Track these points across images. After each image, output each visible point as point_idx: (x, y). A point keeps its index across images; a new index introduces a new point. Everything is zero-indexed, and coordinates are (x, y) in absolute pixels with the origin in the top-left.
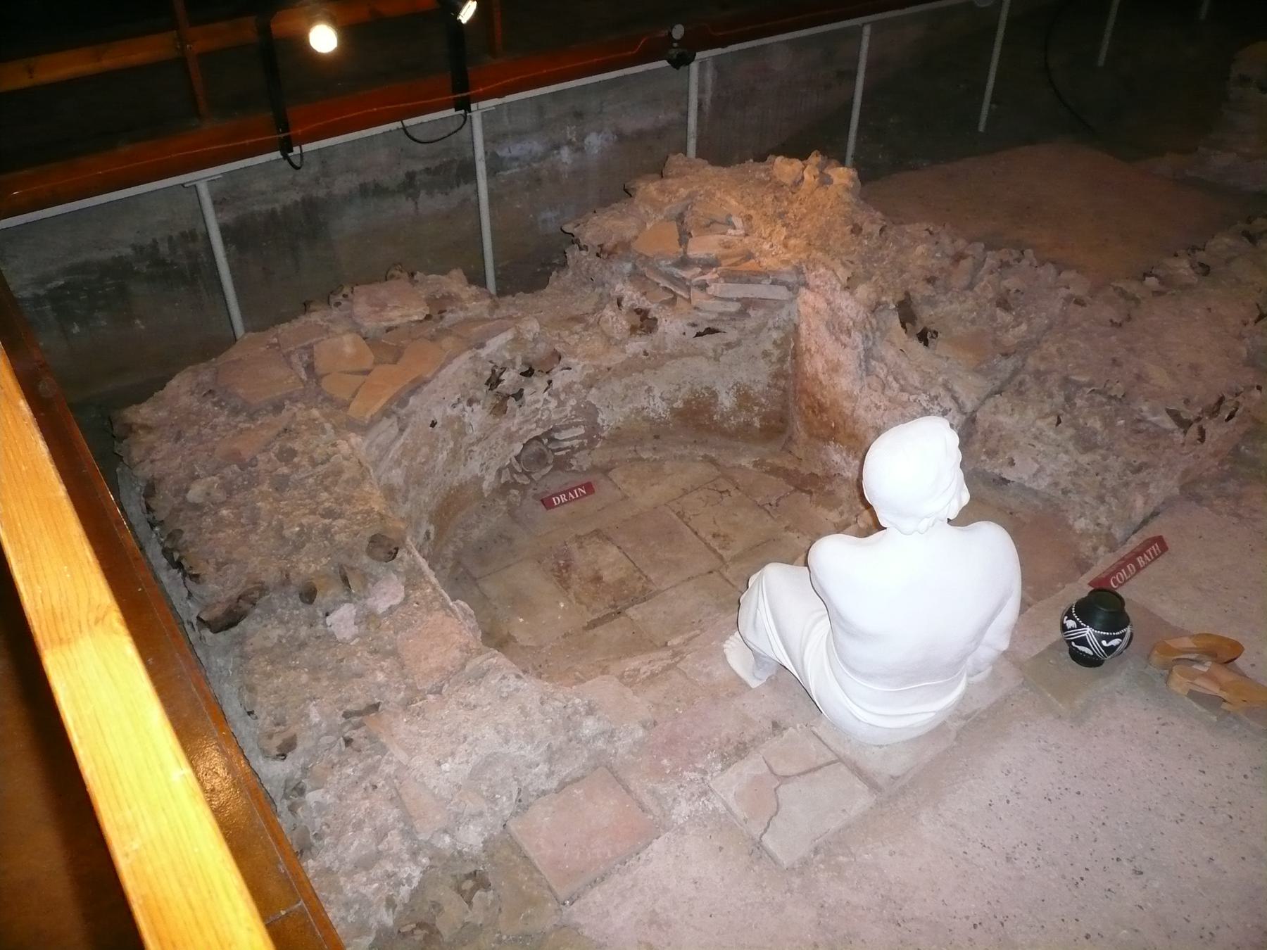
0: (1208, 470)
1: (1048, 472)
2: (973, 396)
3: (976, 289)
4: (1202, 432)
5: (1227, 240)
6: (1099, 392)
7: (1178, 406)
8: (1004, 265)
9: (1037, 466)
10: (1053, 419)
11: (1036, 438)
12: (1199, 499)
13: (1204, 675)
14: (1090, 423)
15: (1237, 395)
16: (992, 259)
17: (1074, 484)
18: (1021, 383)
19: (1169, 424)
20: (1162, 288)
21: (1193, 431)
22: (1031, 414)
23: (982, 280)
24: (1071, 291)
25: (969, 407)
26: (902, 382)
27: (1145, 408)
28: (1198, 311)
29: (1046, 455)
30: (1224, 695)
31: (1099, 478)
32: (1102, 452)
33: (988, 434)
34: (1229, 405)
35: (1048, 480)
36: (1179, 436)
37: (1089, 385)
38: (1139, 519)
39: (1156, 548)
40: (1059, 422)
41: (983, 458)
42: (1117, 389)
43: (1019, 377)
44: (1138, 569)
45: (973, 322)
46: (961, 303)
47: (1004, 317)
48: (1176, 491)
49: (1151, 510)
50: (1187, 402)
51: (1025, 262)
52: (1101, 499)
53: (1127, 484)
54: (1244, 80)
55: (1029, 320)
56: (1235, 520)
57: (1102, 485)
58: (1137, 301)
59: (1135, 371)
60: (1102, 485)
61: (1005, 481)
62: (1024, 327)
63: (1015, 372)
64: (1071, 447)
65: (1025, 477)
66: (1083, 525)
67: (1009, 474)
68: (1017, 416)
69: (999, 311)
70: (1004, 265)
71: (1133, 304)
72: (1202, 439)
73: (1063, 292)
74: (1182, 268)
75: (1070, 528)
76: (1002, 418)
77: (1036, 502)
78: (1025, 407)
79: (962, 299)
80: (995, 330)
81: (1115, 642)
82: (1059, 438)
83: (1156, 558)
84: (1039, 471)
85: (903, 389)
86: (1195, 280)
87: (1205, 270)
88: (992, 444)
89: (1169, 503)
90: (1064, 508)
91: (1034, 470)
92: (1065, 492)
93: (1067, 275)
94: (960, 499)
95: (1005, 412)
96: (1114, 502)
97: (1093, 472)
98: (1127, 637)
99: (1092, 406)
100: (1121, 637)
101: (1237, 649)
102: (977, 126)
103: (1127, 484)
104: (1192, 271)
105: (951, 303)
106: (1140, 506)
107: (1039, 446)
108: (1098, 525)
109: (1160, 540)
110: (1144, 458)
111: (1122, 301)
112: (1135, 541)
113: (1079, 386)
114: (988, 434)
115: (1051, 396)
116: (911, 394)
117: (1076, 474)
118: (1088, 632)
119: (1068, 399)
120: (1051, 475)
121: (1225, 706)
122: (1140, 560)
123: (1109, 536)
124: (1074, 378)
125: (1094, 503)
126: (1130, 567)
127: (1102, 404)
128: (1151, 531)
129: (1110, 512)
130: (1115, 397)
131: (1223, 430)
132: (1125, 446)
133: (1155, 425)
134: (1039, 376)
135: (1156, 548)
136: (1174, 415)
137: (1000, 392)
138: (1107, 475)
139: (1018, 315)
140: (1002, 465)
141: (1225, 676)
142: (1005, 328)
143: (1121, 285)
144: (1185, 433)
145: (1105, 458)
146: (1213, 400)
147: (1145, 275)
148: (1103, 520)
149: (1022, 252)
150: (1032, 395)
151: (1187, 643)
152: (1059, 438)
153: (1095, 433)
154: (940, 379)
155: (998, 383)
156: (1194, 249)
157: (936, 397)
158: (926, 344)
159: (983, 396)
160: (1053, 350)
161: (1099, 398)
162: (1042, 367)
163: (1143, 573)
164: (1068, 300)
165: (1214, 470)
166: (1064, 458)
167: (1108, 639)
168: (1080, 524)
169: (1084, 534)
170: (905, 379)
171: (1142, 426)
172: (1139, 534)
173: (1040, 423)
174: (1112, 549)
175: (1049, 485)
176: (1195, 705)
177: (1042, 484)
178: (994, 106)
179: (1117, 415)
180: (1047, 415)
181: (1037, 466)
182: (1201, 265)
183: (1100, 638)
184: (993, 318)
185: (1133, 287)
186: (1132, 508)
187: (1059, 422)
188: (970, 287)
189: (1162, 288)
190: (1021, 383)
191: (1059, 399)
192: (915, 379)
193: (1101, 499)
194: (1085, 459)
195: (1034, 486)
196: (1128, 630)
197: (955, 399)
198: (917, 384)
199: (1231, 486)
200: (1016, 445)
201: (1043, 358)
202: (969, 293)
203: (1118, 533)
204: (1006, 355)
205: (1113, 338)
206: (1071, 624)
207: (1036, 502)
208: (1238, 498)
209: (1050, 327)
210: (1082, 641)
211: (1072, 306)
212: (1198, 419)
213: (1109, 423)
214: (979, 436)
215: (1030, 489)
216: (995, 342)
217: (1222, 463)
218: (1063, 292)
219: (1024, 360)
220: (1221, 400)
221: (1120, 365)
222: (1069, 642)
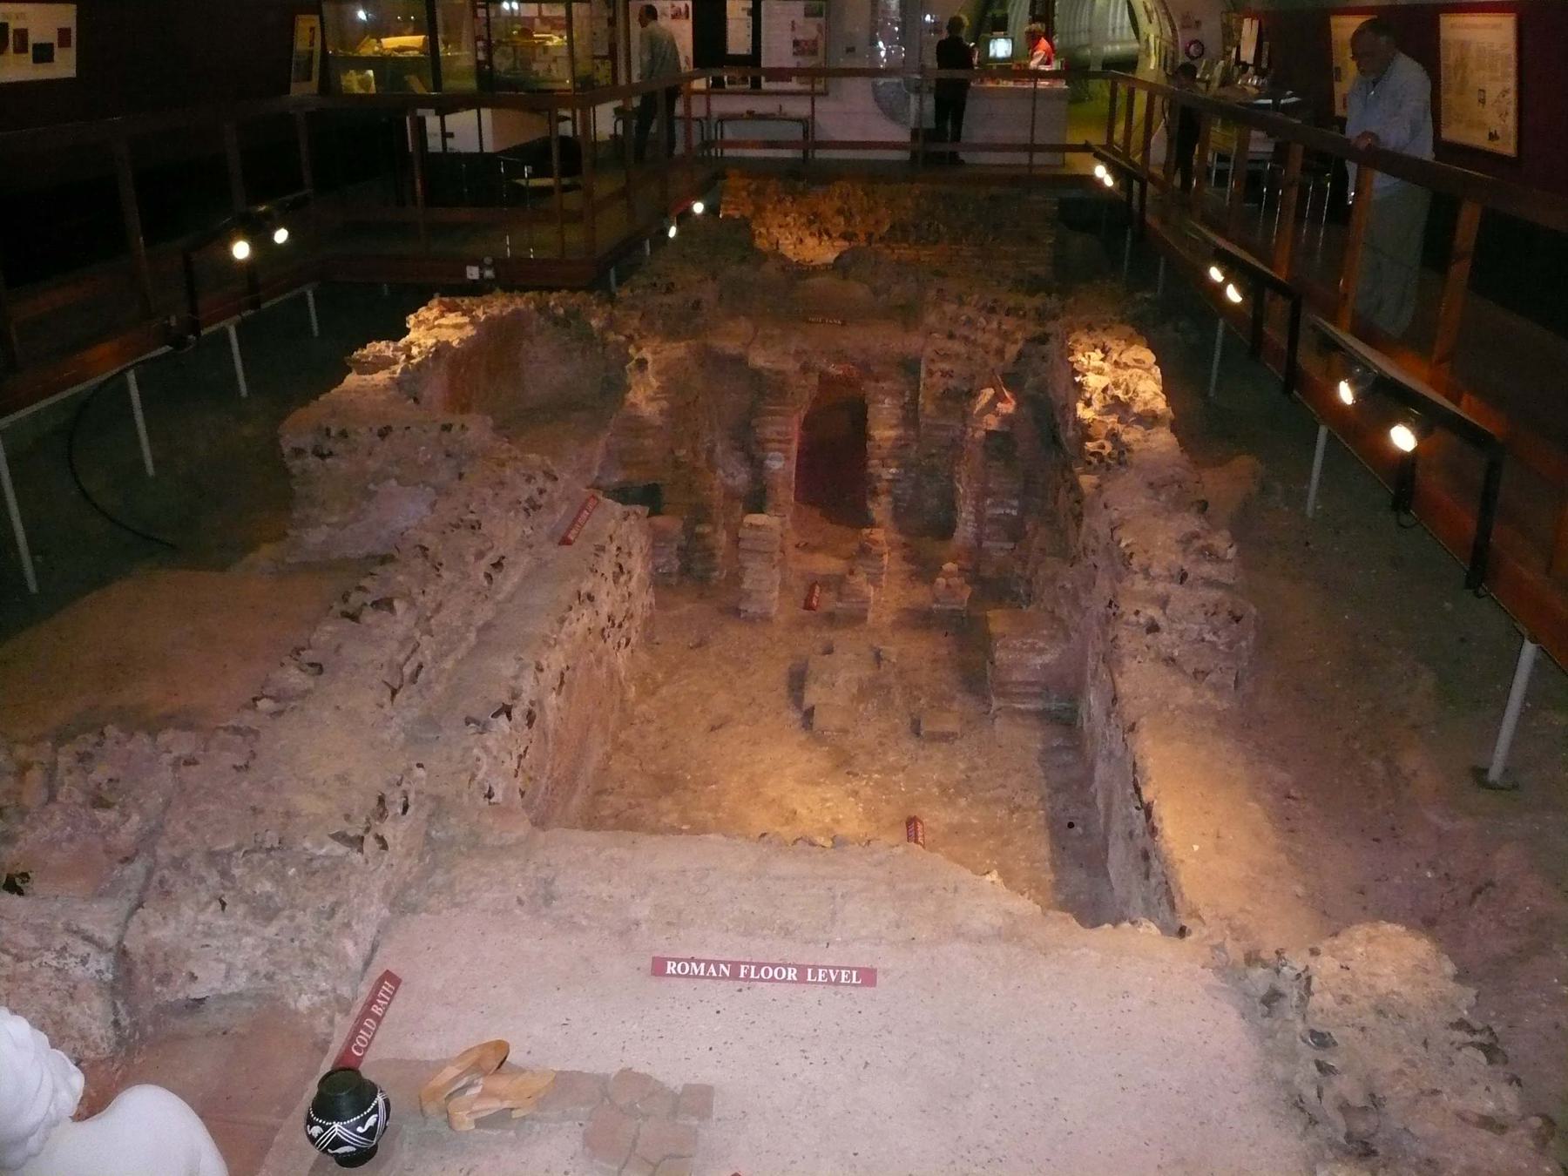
0: (409, 873)
1: (240, 966)
2: (108, 926)
3: (60, 798)
4: (381, 839)
5: (329, 628)
6: (254, 851)
7: (340, 826)
8: (83, 757)
9: (223, 966)
10: (216, 905)
11: (206, 935)
12: (414, 909)
13: (480, 1096)
14: (258, 889)
15: (399, 784)
16: (65, 759)
17: (274, 964)
18: (162, 882)
19: (340, 850)
20: (280, 706)
21: (370, 843)
22: (188, 912)
23: (63, 784)
24: (175, 754)
25: (110, 939)
26: (14, 951)
27: (308, 844)
28: (326, 714)
29: (226, 949)
30: (507, 1104)
31: (297, 943)
32: (287, 913)
33: (149, 960)
34: (395, 798)
35: (245, 974)
36: (356, 857)
37: (238, 848)
38: (359, 965)
39: (387, 986)
40: (224, 904)
41: (157, 989)
42: (271, 839)
43: (156, 878)
44: (378, 1020)
45: (71, 839)
46: (46, 824)
47: (106, 817)
48: (386, 913)
49: (369, 948)
50: (347, 817)
51: (109, 744)
52: (310, 965)
53: (328, 934)
54: (299, 452)
55: (140, 809)
56: (455, 911)
57: (302, 949)
58: (256, 733)
59: (281, 809)
60: (302, 949)
61: (201, 1001)
62: (136, 818)
63: (150, 873)
64: (249, 925)
65: (217, 985)
66: (307, 1003)
67: (197, 991)
68: (173, 924)
69: (100, 814)
70: (83, 757)
71: (251, 737)
72: (385, 846)
73: (167, 758)
74: (294, 678)
75: (296, 1012)
76: (155, 934)
77: (246, 1004)
78: (178, 907)
79: (45, 818)
80: (103, 836)
81: (371, 1121)
82: (232, 922)
83: (392, 997)
84: (228, 972)
85: (18, 958)
86: (311, 683)
87: (318, 668)
88: (160, 968)
89: (384, 929)
90: (278, 994)
91: (223, 973)
92: (269, 977)
93: (166, 737)
94: (70, 1088)
95: (158, 923)
96: (323, 960)
97: (286, 941)
98: (381, 1107)
99: (252, 869)
100: (375, 1110)
101: (502, 1048)
102: (26, 587)
103: (328, 934)
104: (303, 676)
105: (34, 829)
106: (353, 951)
107: (214, 943)
108: (322, 993)
109: (389, 976)
110: (330, 899)
111: (239, 739)
112: (365, 990)
113: (229, 854)
114: (149, 960)
115: (202, 880)
116: (32, 959)
117: (271, 951)
118: (337, 1128)
119: (225, 874)
120: (245, 967)
121: (515, 1114)
122: (376, 1010)
123: (338, 999)
124: (218, 848)
125: (304, 972)
126: (369, 1022)
127: (262, 863)
128: (376, 971)
129: (325, 972)
130: (272, 849)
131: (405, 823)
132: (306, 894)
133: (326, 857)
134: (178, 864)
135: (387, 986)
136: (341, 837)
137: (140, 905)
138: (303, 936)
139: (123, 806)
140: (183, 986)
141: (501, 1084)
142: (114, 828)
143: (231, 723)
144: (361, 850)
145: (292, 918)
146: (374, 802)
147: (255, 699)
148: (324, 985)
149: (102, 734)
150: (180, 889)
151: (451, 1072)
152: (232, 922)
153: (270, 897)
154: (60, 926)
155: (134, 895)
156: (297, 651)
157: (64, 949)
158: (21, 893)
159: (122, 920)
160: (181, 829)
161: (256, 857)
162: (177, 852)
163: (385, 1021)
164: (175, 765)
165: (415, 870)
166: (248, 941)
167: (362, 1122)
168: (304, 1003)
169: (313, 1012)
170: (16, 945)
171: (316, 864)
172: (366, 979)
173: (201, 918)
174: (347, 1012)
175: (249, 980)
176: (488, 1132)
177: (241, 982)
178: (39, 558)
179: (284, 866)
180: (208, 903)
181: (223, 966)
182: (312, 665)
183: (353, 1128)
184: (95, 823)
185: (248, 719)
186: (346, 956)
187: (224, 904)
188: (52, 798)
189: (280, 706)
190: (162, 882)
191: (214, 879)
192: (28, 940)
193: (310, 965)
194: (271, 931)
195: (232, 989)
196: (379, 1099)
197: (88, 939)
198: (34, 944)
199: (439, 878)
200: (188, 955)
201: (173, 844)
202: (52, 807)
203: (345, 991)
204: (127, 860)
205: (245, 785)
206: (316, 1130)
207: (246, 1004)
208: (450, 885)
209: (168, 804)
210: (338, 1142)
211: (183, 769)
212: (368, 830)
213: (280, 878)
214: (140, 967)
215: (232, 995)
216: (108, 851)
217: (421, 859)
218: (167, 758)
219: (154, 856)
220: (381, 800)
221: (262, 812)
222: (325, 1151)
